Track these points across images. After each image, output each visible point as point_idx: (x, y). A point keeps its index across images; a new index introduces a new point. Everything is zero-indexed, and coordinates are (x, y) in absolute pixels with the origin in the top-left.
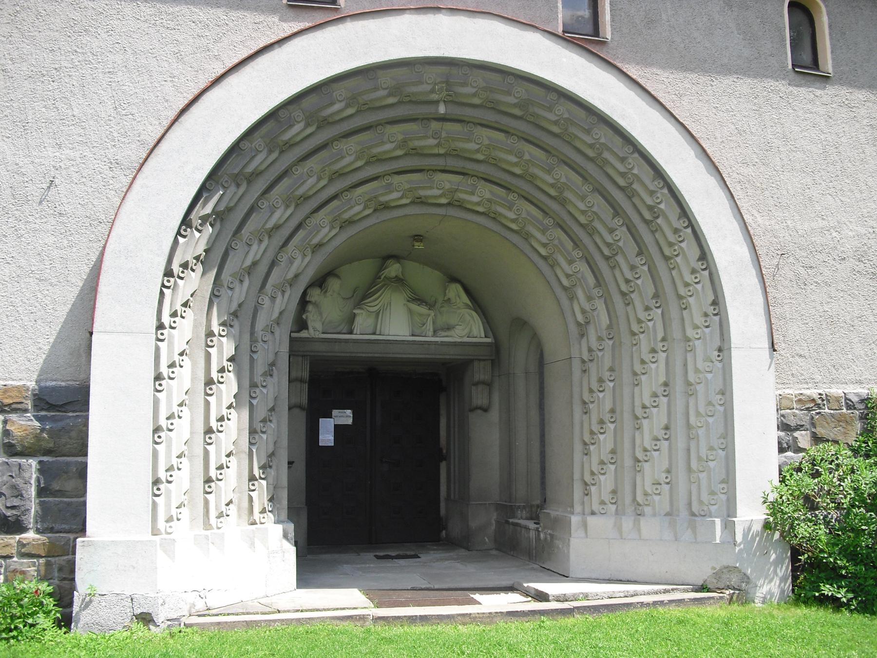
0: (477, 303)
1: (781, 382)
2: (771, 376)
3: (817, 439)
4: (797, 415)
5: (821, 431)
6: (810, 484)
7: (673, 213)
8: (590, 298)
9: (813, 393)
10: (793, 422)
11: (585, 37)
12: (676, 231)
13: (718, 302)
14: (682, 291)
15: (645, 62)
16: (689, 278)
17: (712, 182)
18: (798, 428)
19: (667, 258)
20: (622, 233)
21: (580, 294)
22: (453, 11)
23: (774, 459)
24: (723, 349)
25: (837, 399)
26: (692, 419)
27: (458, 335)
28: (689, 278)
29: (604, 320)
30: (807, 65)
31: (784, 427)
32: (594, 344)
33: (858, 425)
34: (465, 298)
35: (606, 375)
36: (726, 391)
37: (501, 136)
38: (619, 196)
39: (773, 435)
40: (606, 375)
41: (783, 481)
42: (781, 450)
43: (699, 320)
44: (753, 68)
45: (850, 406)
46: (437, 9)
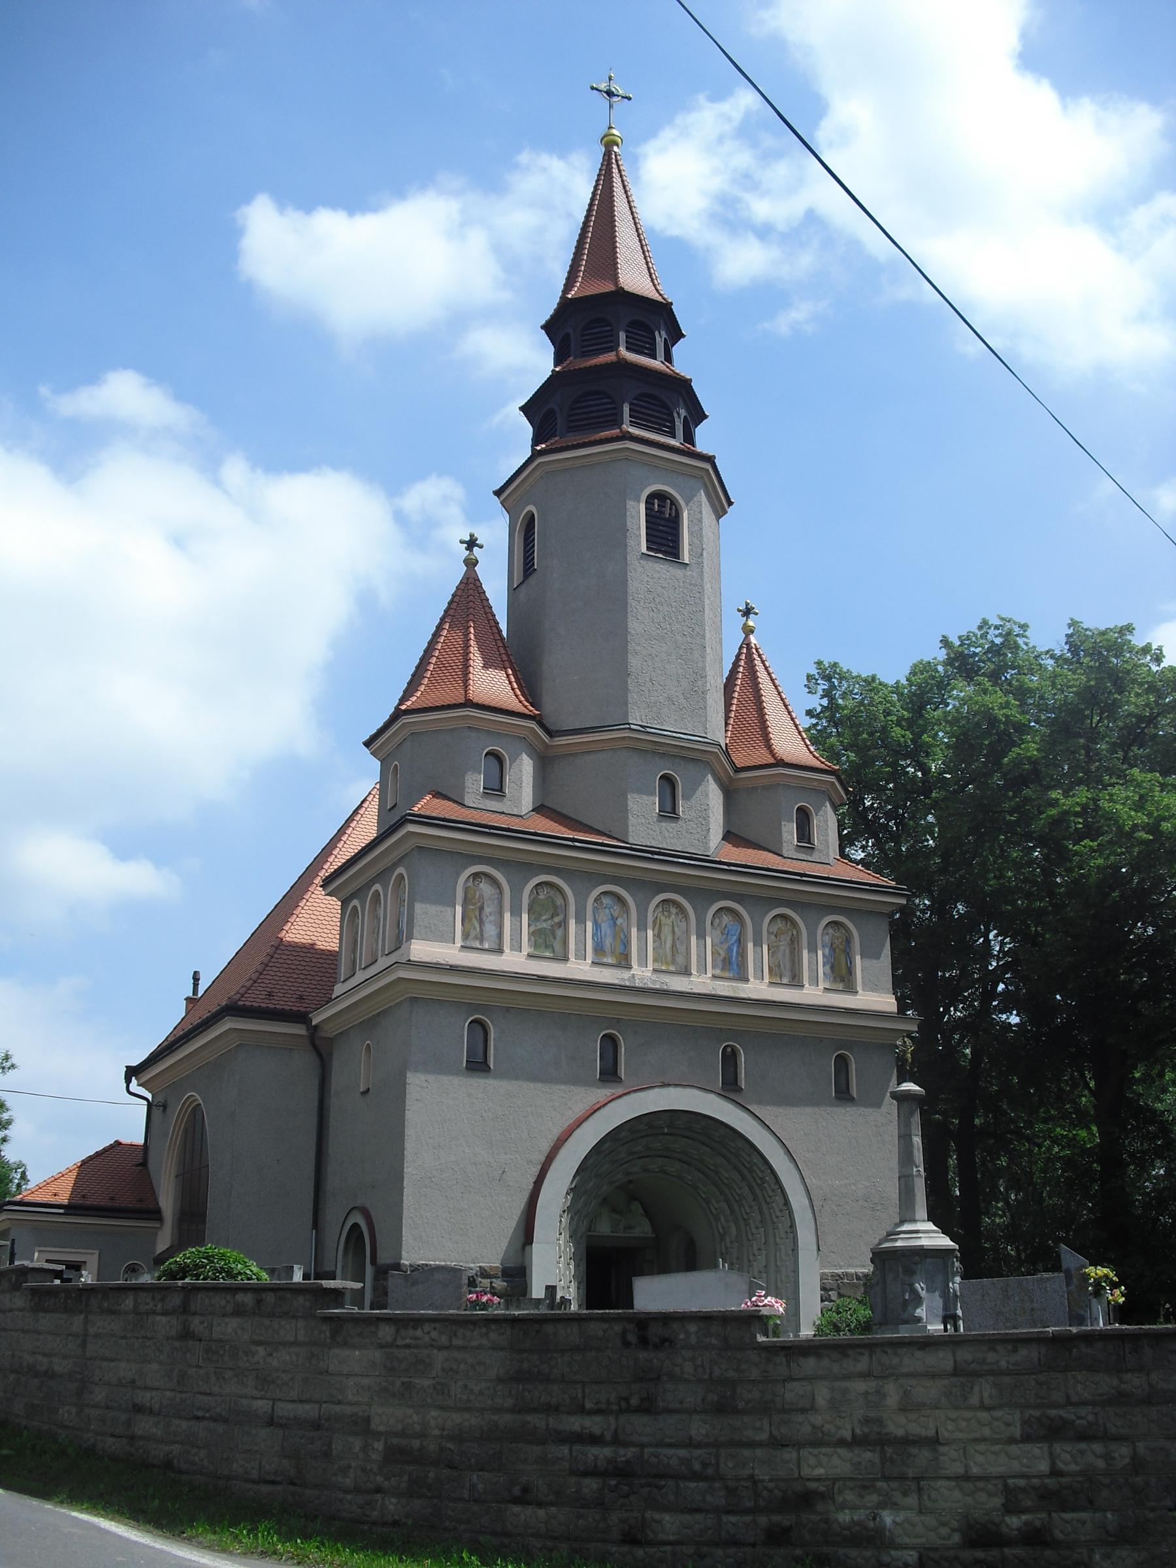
0: (647, 1213)
1: (822, 1266)
2: (818, 1263)
3: (840, 1295)
4: (830, 1282)
5: (842, 1291)
6: (836, 1317)
7: (772, 1182)
8: (727, 1221)
9: (839, 1271)
10: (828, 1286)
11: (730, 1087)
12: (773, 1190)
13: (793, 1226)
14: (775, 1220)
15: (760, 1102)
16: (778, 1214)
17: (792, 1166)
18: (831, 1290)
19: (767, 1203)
20: (746, 1190)
21: (722, 1219)
22: (676, 1085)
23: (818, 1305)
24: (795, 1249)
25: (852, 1275)
26: (779, 1284)
27: (637, 1232)
28: (778, 1214)
29: (734, 1231)
30: (844, 1095)
31: (823, 1289)
32: (729, 1245)
33: (862, 1289)
34: (641, 1210)
35: (735, 1261)
36: (796, 1271)
37: (690, 1141)
38: (745, 1171)
39: (818, 1293)
40: (735, 1261)
41: (823, 1315)
42: (822, 1301)
43: (783, 1235)
44: (814, 1100)
45: (858, 1278)
46: (669, 1085)
